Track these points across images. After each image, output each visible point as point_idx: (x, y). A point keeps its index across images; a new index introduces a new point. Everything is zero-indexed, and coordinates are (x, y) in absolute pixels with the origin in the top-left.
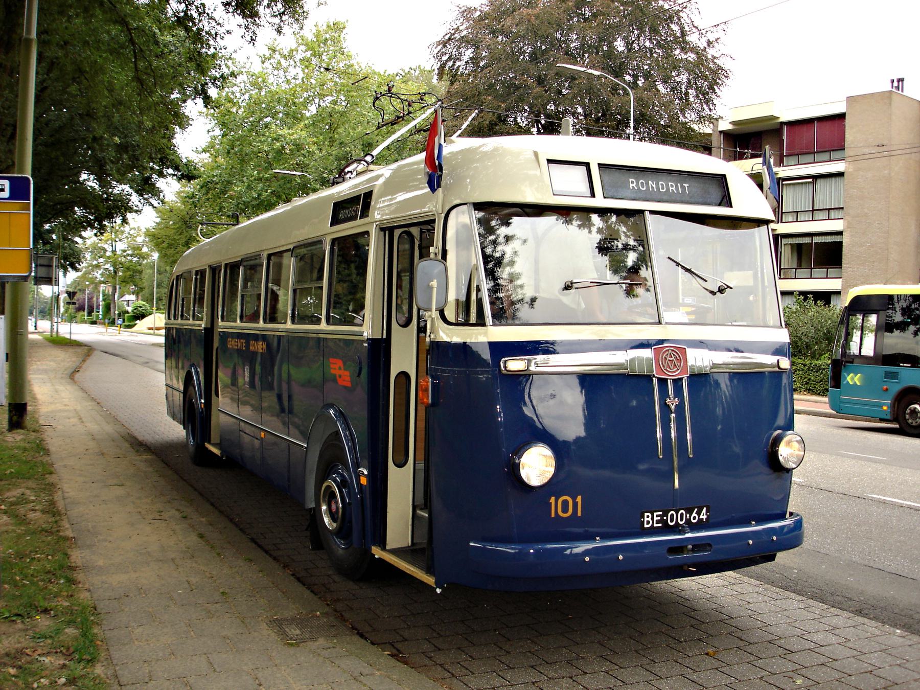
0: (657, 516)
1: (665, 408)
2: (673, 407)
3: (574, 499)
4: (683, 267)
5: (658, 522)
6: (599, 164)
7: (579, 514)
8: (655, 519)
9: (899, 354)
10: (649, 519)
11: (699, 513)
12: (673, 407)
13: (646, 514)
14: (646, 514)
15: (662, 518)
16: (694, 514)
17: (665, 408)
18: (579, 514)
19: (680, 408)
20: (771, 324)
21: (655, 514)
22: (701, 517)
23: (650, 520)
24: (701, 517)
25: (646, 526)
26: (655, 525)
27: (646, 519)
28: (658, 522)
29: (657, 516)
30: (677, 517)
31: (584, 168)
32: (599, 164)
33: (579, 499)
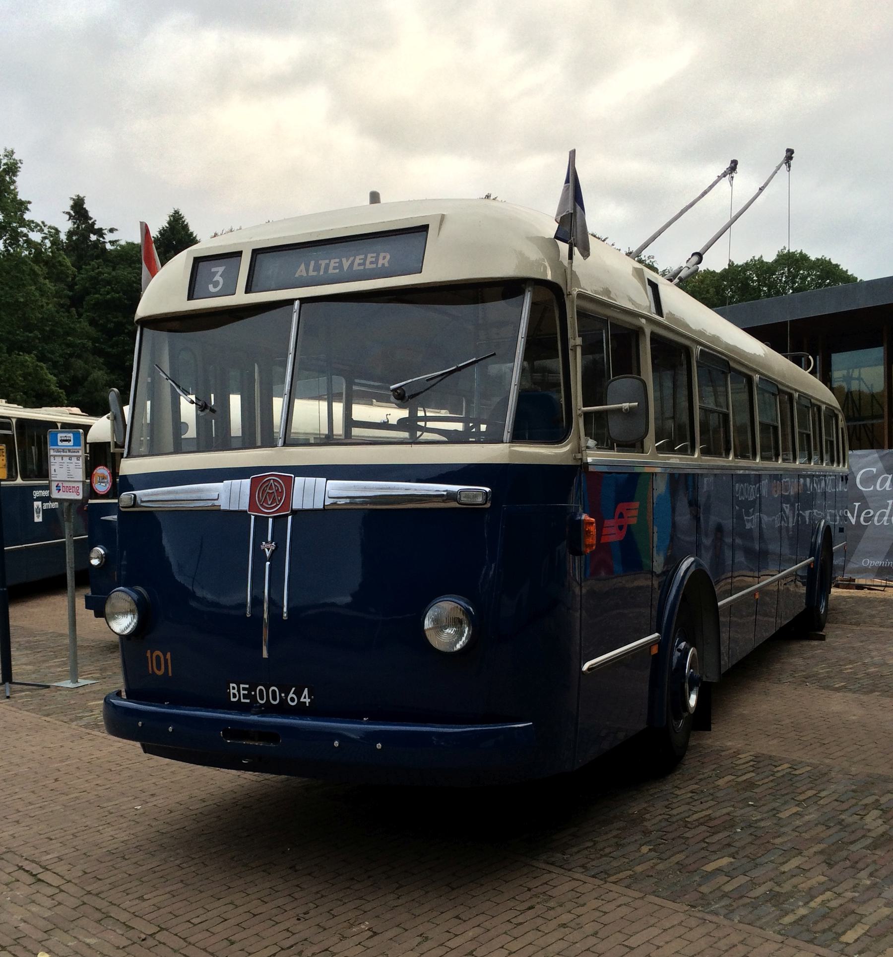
0: (244, 689)
1: (259, 554)
2: (268, 553)
3: (165, 656)
4: (422, 392)
5: (245, 697)
6: (188, 299)
7: (170, 674)
8: (242, 692)
9: (217, 327)
10: (235, 691)
11: (299, 694)
12: (268, 553)
13: (232, 685)
14: (232, 685)
15: (249, 693)
16: (291, 695)
17: (259, 554)
18: (170, 674)
19: (277, 557)
20: (716, 415)
21: (242, 686)
22: (302, 700)
23: (236, 692)
24: (302, 700)
25: (233, 700)
26: (243, 700)
27: (232, 691)
28: (245, 697)
29: (244, 689)
30: (271, 694)
31: (202, 265)
32: (188, 299)
33: (168, 656)
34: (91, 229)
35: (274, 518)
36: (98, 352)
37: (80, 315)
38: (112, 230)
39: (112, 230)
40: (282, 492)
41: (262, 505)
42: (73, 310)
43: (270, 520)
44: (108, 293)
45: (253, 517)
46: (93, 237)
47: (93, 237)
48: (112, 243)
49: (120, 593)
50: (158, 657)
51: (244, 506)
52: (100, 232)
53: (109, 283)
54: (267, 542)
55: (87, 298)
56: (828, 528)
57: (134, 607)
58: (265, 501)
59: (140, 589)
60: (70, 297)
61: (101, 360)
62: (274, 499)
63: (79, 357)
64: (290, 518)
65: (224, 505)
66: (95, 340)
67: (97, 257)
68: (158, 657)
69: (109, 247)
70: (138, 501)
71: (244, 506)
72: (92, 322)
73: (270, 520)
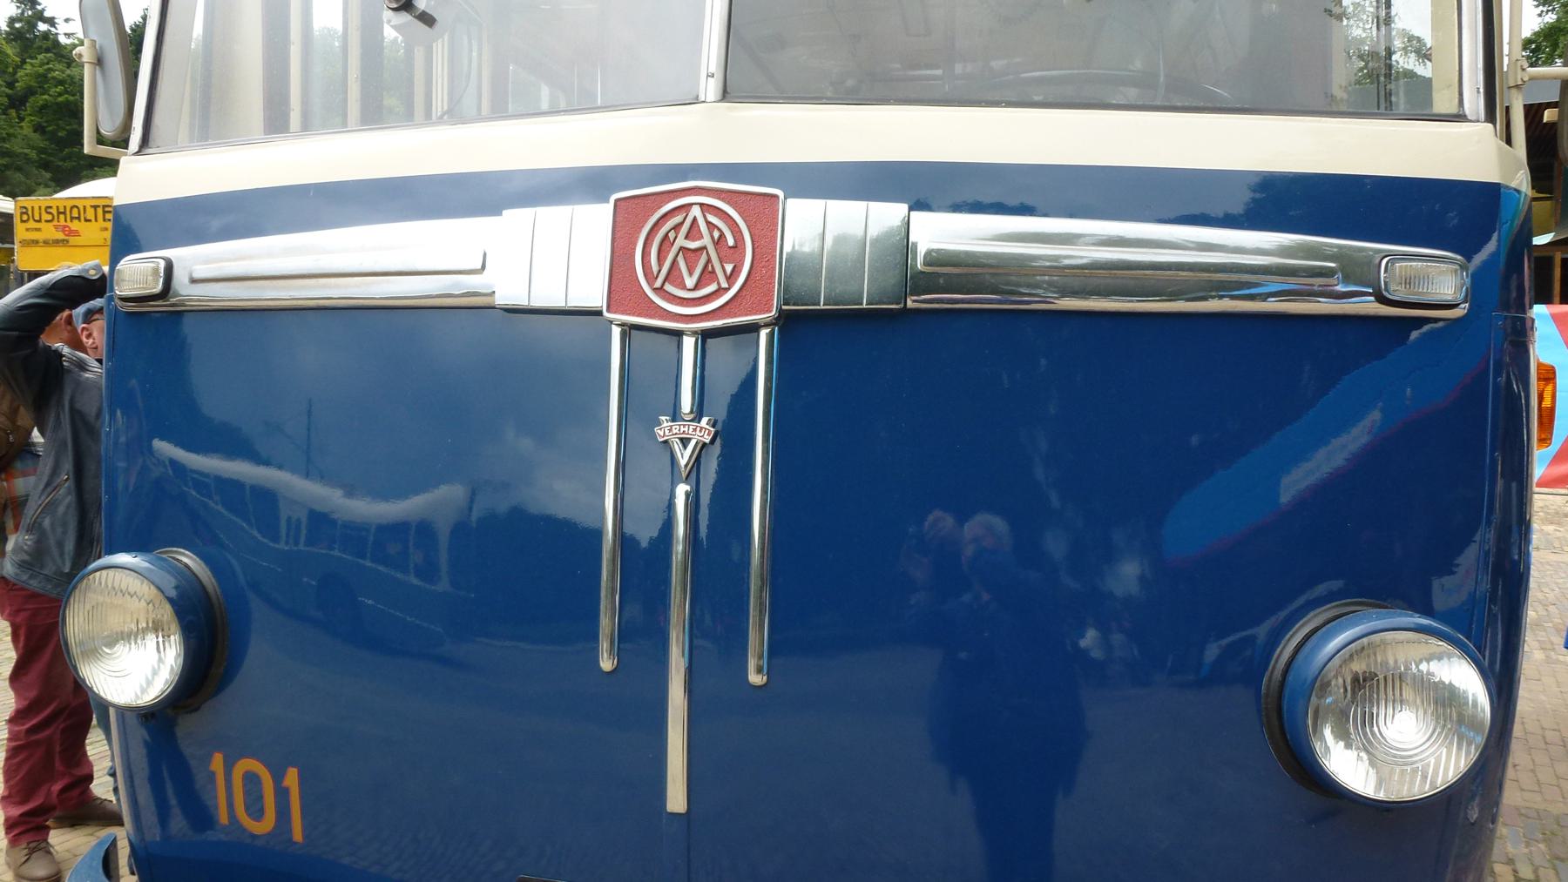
2: (684, 457)
3: (278, 777)
7: (298, 835)
33: (292, 778)
34: (40, 16)
35: (706, 335)
36: (45, 166)
37: (22, 119)
38: (67, 20)
39: (67, 20)
40: (739, 245)
41: (659, 290)
42: (13, 112)
43: (689, 343)
44: (60, 94)
45: (616, 332)
46: (42, 27)
47: (42, 27)
48: (68, 35)
49: (118, 574)
50: (251, 779)
51: (591, 291)
52: (51, 21)
53: (61, 82)
54: (675, 416)
55: (32, 99)
56: (698, 419)
57: (167, 612)
58: (673, 275)
59: (188, 558)
60: (8, 96)
61: (48, 175)
62: (707, 275)
63: (19, 169)
64: (764, 333)
65: (508, 287)
66: (41, 151)
67: (48, 50)
68: (251, 779)
69: (63, 40)
70: (180, 278)
71: (591, 291)
72: (39, 129)
73: (689, 343)
